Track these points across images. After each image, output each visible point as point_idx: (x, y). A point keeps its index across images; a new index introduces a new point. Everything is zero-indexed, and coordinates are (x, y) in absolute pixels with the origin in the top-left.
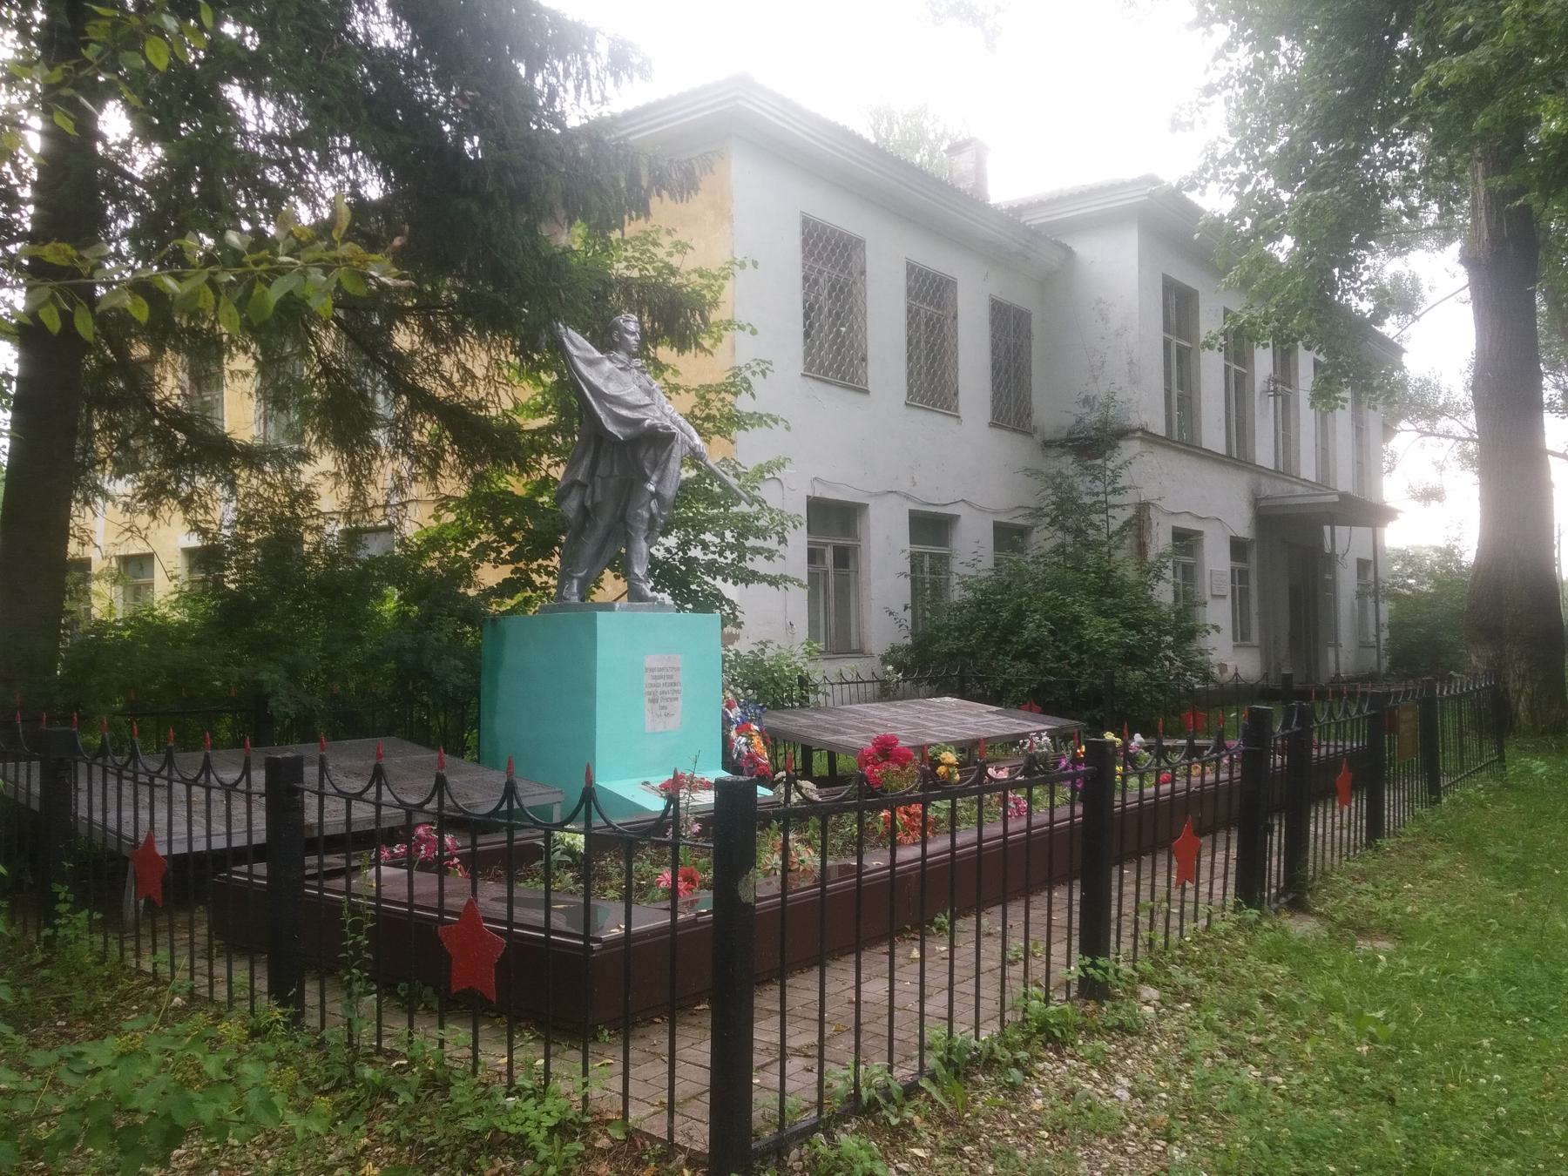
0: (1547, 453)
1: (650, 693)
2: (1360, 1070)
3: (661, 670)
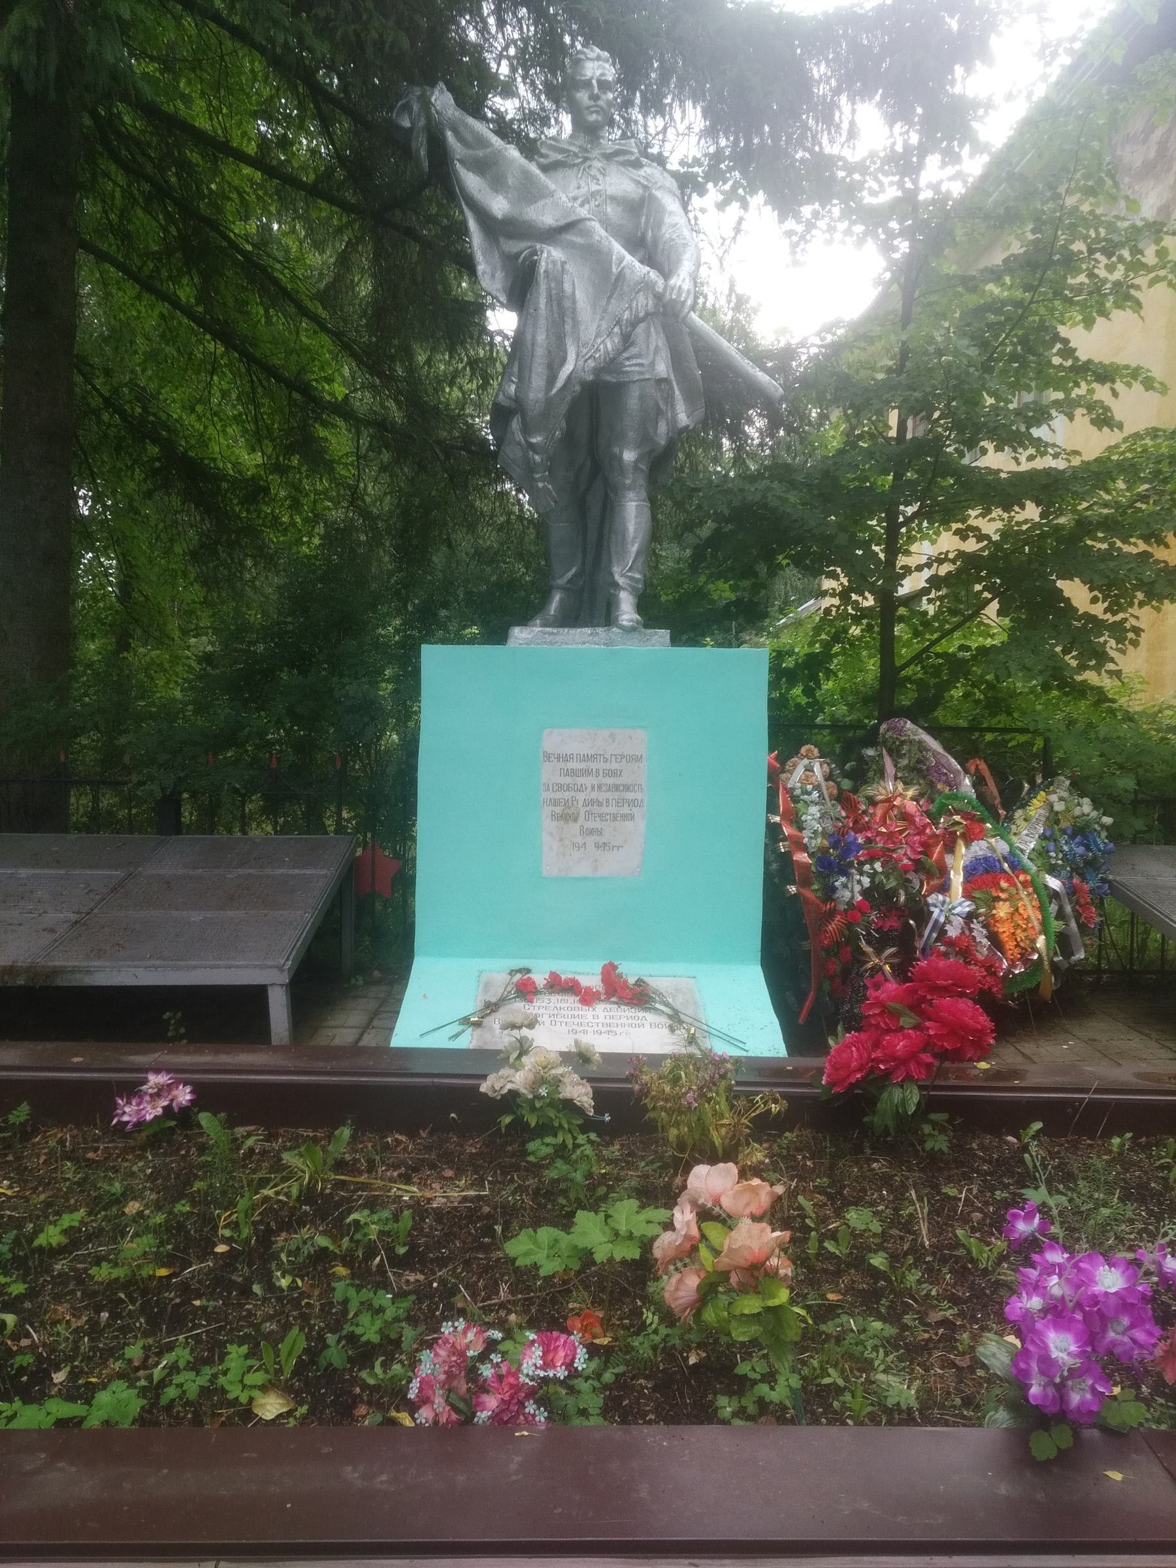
0: (218, 1561)
1: (555, 803)
2: (730, 183)
3: (586, 758)
